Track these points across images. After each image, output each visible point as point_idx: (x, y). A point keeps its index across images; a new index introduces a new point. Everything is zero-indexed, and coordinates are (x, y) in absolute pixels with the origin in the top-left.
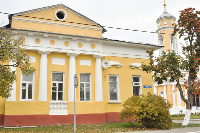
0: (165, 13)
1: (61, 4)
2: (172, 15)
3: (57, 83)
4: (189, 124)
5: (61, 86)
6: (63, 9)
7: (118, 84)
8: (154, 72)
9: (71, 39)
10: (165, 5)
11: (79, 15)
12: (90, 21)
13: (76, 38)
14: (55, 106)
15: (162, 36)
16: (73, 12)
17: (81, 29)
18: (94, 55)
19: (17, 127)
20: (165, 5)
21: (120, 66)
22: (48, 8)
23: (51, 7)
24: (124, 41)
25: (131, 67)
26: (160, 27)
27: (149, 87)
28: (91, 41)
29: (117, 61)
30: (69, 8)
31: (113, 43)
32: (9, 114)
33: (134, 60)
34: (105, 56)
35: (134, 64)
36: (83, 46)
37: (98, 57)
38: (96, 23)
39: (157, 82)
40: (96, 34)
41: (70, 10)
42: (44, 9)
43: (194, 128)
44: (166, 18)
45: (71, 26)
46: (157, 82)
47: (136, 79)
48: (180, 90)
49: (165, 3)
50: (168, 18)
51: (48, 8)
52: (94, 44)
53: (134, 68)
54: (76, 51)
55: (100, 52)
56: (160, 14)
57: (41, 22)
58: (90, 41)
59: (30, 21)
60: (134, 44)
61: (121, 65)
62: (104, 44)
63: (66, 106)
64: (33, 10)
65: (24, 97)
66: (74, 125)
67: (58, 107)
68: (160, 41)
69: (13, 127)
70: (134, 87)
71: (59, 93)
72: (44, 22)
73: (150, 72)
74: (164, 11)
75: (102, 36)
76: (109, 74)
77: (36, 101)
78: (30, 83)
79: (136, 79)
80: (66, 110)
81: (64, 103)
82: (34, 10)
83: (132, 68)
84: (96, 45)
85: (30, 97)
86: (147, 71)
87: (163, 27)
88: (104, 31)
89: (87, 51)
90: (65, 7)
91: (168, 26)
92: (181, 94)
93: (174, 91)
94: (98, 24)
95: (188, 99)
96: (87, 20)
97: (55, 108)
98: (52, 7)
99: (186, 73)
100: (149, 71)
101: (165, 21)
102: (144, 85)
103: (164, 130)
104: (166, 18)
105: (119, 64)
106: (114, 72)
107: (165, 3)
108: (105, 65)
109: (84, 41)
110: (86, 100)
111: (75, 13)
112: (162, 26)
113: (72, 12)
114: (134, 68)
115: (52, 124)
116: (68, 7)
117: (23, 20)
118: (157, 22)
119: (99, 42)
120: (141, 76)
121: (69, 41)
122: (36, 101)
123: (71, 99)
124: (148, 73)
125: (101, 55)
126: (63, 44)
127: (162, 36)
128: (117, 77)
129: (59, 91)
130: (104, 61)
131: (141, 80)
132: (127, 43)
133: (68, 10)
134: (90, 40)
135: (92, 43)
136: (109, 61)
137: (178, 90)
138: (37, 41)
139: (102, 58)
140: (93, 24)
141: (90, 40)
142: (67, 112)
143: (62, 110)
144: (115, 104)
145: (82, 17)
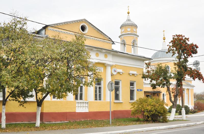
0: (129, 20)
1: (85, 19)
2: (134, 23)
3: (98, 86)
4: (174, 120)
5: (100, 88)
6: (85, 23)
7: (120, 87)
8: (150, 80)
9: (91, 49)
10: (128, 13)
11: (97, 30)
12: (104, 35)
13: (96, 49)
14: (79, 105)
15: (124, 41)
16: (93, 27)
17: (97, 41)
18: (106, 63)
19: (53, 123)
20: (128, 13)
21: (137, 75)
22: (72, 22)
23: (77, 21)
24: (127, 54)
25: (129, 74)
26: (124, 33)
27: (141, 90)
28: (97, 50)
29: (120, 69)
30: (90, 23)
31: (120, 54)
32: (47, 111)
33: (131, 68)
34: (114, 64)
35: (132, 72)
36: (99, 56)
37: (109, 65)
38: (108, 37)
39: (152, 87)
40: (106, 46)
41: (90, 25)
42: (72, 22)
43: (177, 122)
44: (130, 25)
45: (91, 39)
46: (152, 87)
47: (132, 84)
48: (170, 94)
49: (128, 11)
50: (132, 25)
51: (72, 22)
52: (98, 54)
53: (131, 75)
54: (95, 59)
55: (110, 62)
56: (123, 20)
57: (70, 33)
58: (104, 52)
59: (62, 32)
60: (133, 56)
61: (124, 72)
62: (113, 55)
63: (87, 105)
64: (64, 22)
65: (96, 99)
66: (110, 119)
67: (81, 106)
68: (122, 45)
69: (50, 122)
70: (131, 90)
71: (80, 94)
72: (72, 34)
73: (147, 79)
74: (127, 19)
75: (112, 48)
76: (115, 79)
77: (65, 100)
78: (100, 86)
79: (132, 84)
80: (86, 108)
81: (85, 102)
82: (64, 23)
83: (131, 75)
84: (108, 56)
85: (100, 99)
86: (145, 79)
87: (126, 33)
88: (113, 43)
89: (102, 60)
90: (87, 22)
91: (131, 33)
92: (170, 97)
93: (166, 95)
94: (109, 38)
95: (174, 101)
96: (106, 37)
97: (84, 107)
98: (77, 21)
99: (173, 82)
100: (146, 79)
101: (129, 28)
102: (138, 89)
103: (165, 122)
104: (130, 25)
105: (136, 73)
106: (118, 78)
107: (128, 11)
108: (114, 72)
109: (100, 51)
110: (99, 100)
111: (98, 31)
112: (126, 32)
113: (91, 26)
114: (131, 75)
115: (78, 120)
116: (89, 22)
117: (56, 31)
118: (121, 28)
119: (93, 50)
120: (135, 81)
121: (99, 53)
122: (65, 100)
123: (108, 100)
124: (146, 80)
125: (111, 63)
126: (95, 54)
127: (124, 42)
128: (119, 82)
129: (80, 92)
130: (113, 69)
131: (135, 84)
132: (129, 55)
133: (89, 24)
134: (105, 51)
135: (105, 54)
136: (117, 69)
137: (168, 94)
138: (106, 56)
139: (111, 66)
140: (107, 39)
141: (105, 51)
142: (88, 109)
143: (84, 108)
144: (119, 103)
145: (99, 31)
